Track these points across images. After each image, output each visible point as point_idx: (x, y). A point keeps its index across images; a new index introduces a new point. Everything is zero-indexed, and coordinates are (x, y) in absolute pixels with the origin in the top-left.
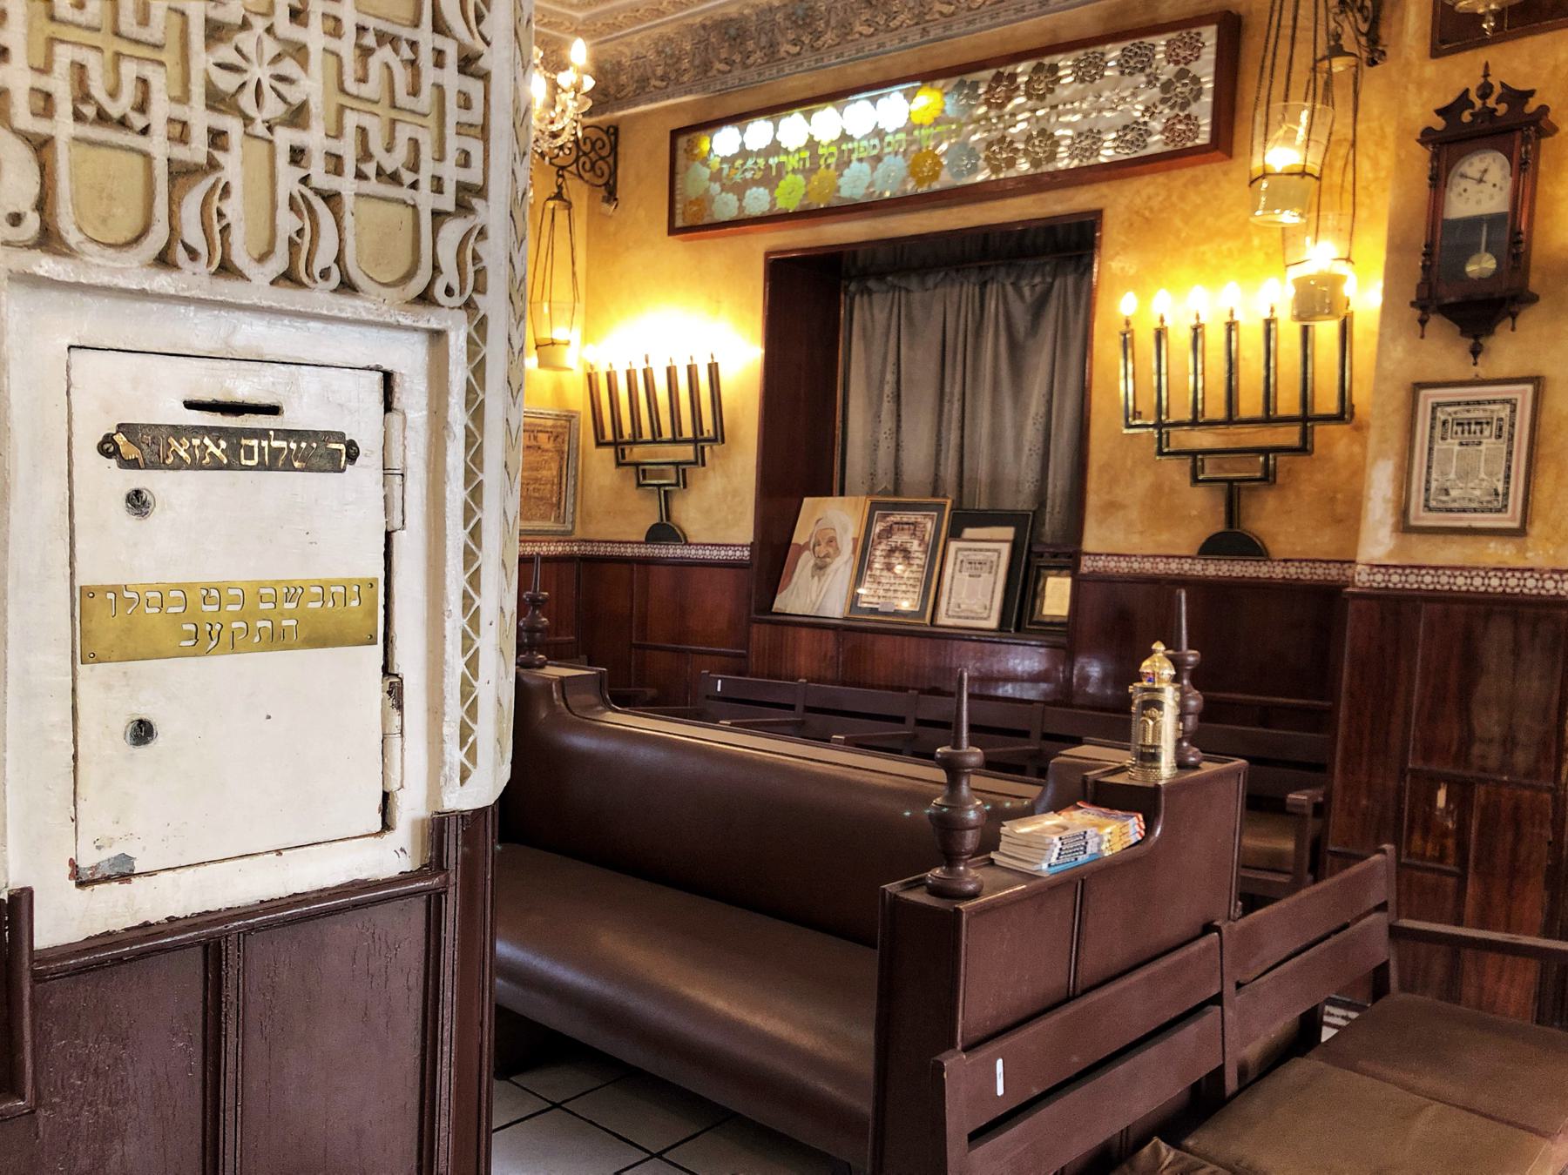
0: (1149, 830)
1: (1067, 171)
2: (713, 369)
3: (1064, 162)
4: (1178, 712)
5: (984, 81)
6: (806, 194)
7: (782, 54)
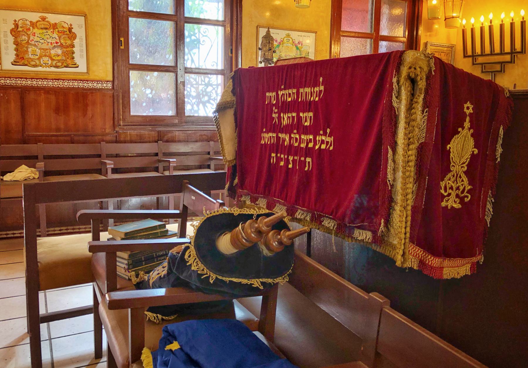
2: (523, 23)
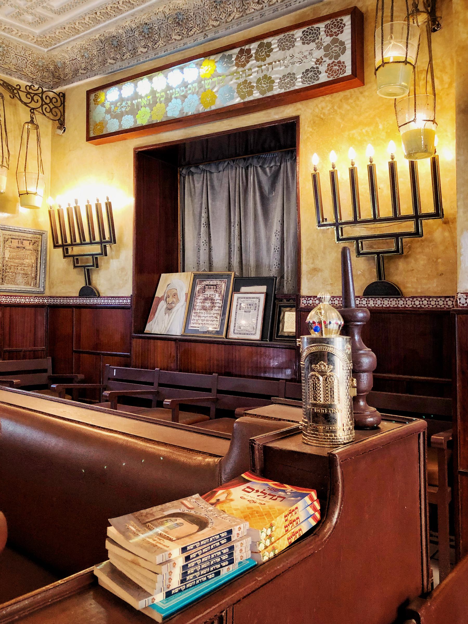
0: (325, 512)
1: (279, 95)
3: (277, 90)
4: (351, 366)
5: (234, 54)
6: (151, 117)
7: (139, 53)
